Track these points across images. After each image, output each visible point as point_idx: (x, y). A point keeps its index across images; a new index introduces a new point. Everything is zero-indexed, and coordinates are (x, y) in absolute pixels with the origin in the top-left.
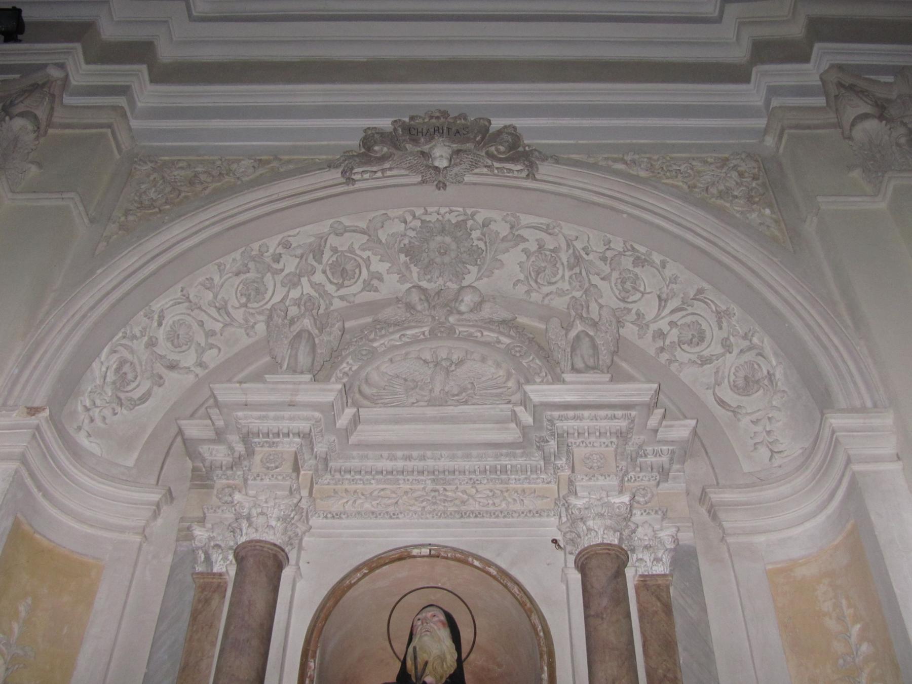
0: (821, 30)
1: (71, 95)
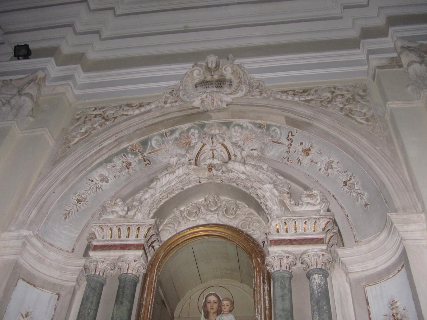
0: (394, 21)
1: (50, 81)
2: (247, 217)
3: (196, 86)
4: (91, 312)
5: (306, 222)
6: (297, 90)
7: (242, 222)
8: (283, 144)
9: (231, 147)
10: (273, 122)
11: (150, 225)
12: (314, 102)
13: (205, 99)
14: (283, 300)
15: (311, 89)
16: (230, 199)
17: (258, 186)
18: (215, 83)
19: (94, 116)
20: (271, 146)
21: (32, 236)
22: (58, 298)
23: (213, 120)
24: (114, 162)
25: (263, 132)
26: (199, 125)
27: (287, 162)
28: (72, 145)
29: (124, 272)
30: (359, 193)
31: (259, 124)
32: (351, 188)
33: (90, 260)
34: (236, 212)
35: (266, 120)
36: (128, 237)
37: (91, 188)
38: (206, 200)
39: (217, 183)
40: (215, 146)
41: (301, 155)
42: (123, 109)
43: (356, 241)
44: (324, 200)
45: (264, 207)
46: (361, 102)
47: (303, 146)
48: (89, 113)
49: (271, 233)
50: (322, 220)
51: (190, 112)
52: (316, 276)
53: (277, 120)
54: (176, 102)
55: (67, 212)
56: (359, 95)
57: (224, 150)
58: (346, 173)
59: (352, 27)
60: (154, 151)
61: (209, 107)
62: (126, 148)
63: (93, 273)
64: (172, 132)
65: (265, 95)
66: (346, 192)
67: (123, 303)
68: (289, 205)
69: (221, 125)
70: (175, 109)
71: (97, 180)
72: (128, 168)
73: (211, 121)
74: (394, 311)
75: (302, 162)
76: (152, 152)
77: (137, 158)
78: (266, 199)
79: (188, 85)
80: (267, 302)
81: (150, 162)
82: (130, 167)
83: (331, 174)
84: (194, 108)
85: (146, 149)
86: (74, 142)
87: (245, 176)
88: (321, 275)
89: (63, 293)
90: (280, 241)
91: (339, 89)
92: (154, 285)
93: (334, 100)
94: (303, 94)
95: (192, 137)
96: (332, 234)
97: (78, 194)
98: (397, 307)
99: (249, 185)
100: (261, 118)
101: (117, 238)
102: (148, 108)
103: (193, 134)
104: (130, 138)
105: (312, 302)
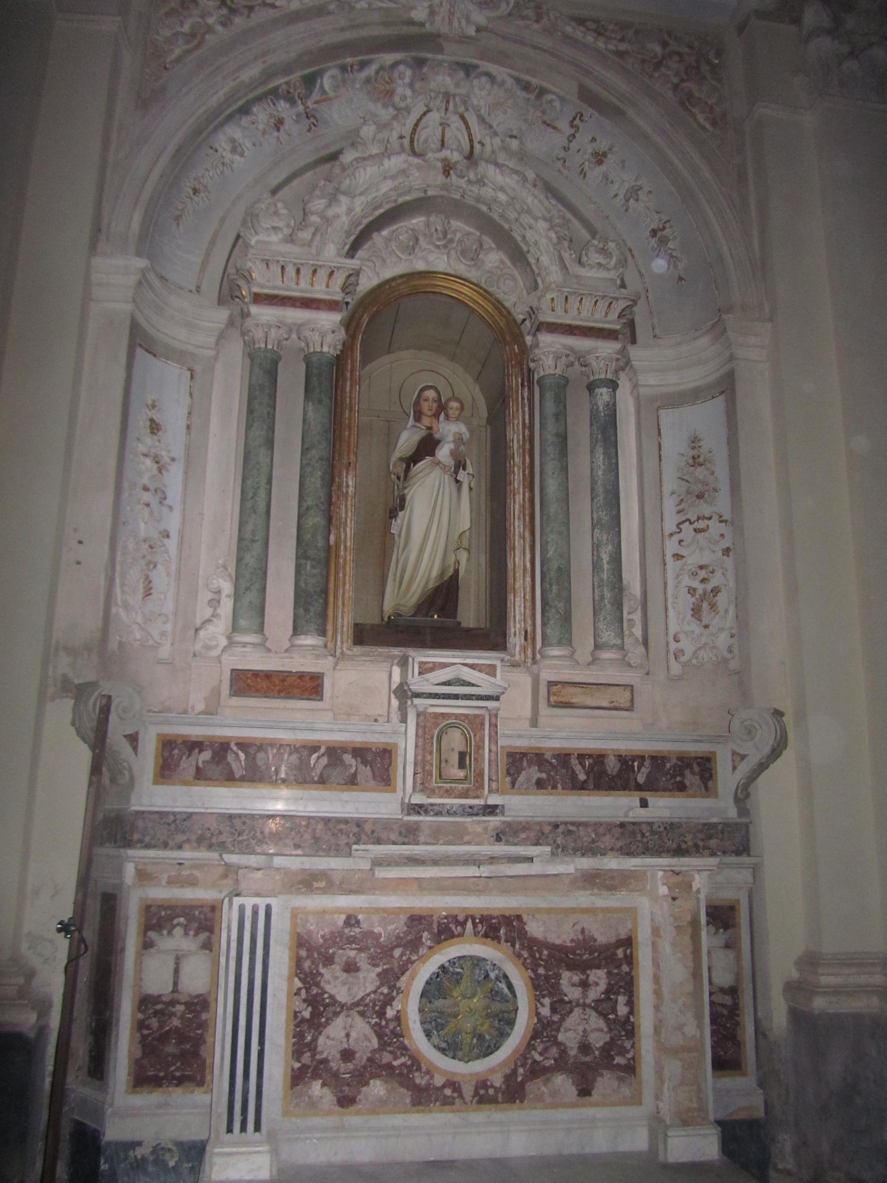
5: (597, 301)
6: (603, 23)
9: (476, 124)
11: (353, 269)
14: (557, 420)
16: (472, 230)
22: (192, 377)
26: (415, 59)
27: (562, 169)
28: (171, 62)
32: (663, 241)
36: (312, 285)
38: (428, 225)
40: (448, 119)
41: (588, 160)
43: (655, 336)
44: (622, 263)
45: (532, 261)
47: (593, 144)
51: (405, 30)
52: (604, 390)
55: (178, 213)
61: (445, 30)
62: (277, 88)
63: (263, 346)
64: (363, 65)
65: (545, 21)
66: (653, 248)
71: (224, 150)
72: (278, 130)
73: (439, 57)
74: (696, 452)
75: (588, 174)
77: (295, 110)
80: (527, 417)
84: (411, 22)
85: (311, 92)
86: (174, 56)
89: (198, 368)
95: (400, 82)
103: (401, 76)
104: (287, 69)
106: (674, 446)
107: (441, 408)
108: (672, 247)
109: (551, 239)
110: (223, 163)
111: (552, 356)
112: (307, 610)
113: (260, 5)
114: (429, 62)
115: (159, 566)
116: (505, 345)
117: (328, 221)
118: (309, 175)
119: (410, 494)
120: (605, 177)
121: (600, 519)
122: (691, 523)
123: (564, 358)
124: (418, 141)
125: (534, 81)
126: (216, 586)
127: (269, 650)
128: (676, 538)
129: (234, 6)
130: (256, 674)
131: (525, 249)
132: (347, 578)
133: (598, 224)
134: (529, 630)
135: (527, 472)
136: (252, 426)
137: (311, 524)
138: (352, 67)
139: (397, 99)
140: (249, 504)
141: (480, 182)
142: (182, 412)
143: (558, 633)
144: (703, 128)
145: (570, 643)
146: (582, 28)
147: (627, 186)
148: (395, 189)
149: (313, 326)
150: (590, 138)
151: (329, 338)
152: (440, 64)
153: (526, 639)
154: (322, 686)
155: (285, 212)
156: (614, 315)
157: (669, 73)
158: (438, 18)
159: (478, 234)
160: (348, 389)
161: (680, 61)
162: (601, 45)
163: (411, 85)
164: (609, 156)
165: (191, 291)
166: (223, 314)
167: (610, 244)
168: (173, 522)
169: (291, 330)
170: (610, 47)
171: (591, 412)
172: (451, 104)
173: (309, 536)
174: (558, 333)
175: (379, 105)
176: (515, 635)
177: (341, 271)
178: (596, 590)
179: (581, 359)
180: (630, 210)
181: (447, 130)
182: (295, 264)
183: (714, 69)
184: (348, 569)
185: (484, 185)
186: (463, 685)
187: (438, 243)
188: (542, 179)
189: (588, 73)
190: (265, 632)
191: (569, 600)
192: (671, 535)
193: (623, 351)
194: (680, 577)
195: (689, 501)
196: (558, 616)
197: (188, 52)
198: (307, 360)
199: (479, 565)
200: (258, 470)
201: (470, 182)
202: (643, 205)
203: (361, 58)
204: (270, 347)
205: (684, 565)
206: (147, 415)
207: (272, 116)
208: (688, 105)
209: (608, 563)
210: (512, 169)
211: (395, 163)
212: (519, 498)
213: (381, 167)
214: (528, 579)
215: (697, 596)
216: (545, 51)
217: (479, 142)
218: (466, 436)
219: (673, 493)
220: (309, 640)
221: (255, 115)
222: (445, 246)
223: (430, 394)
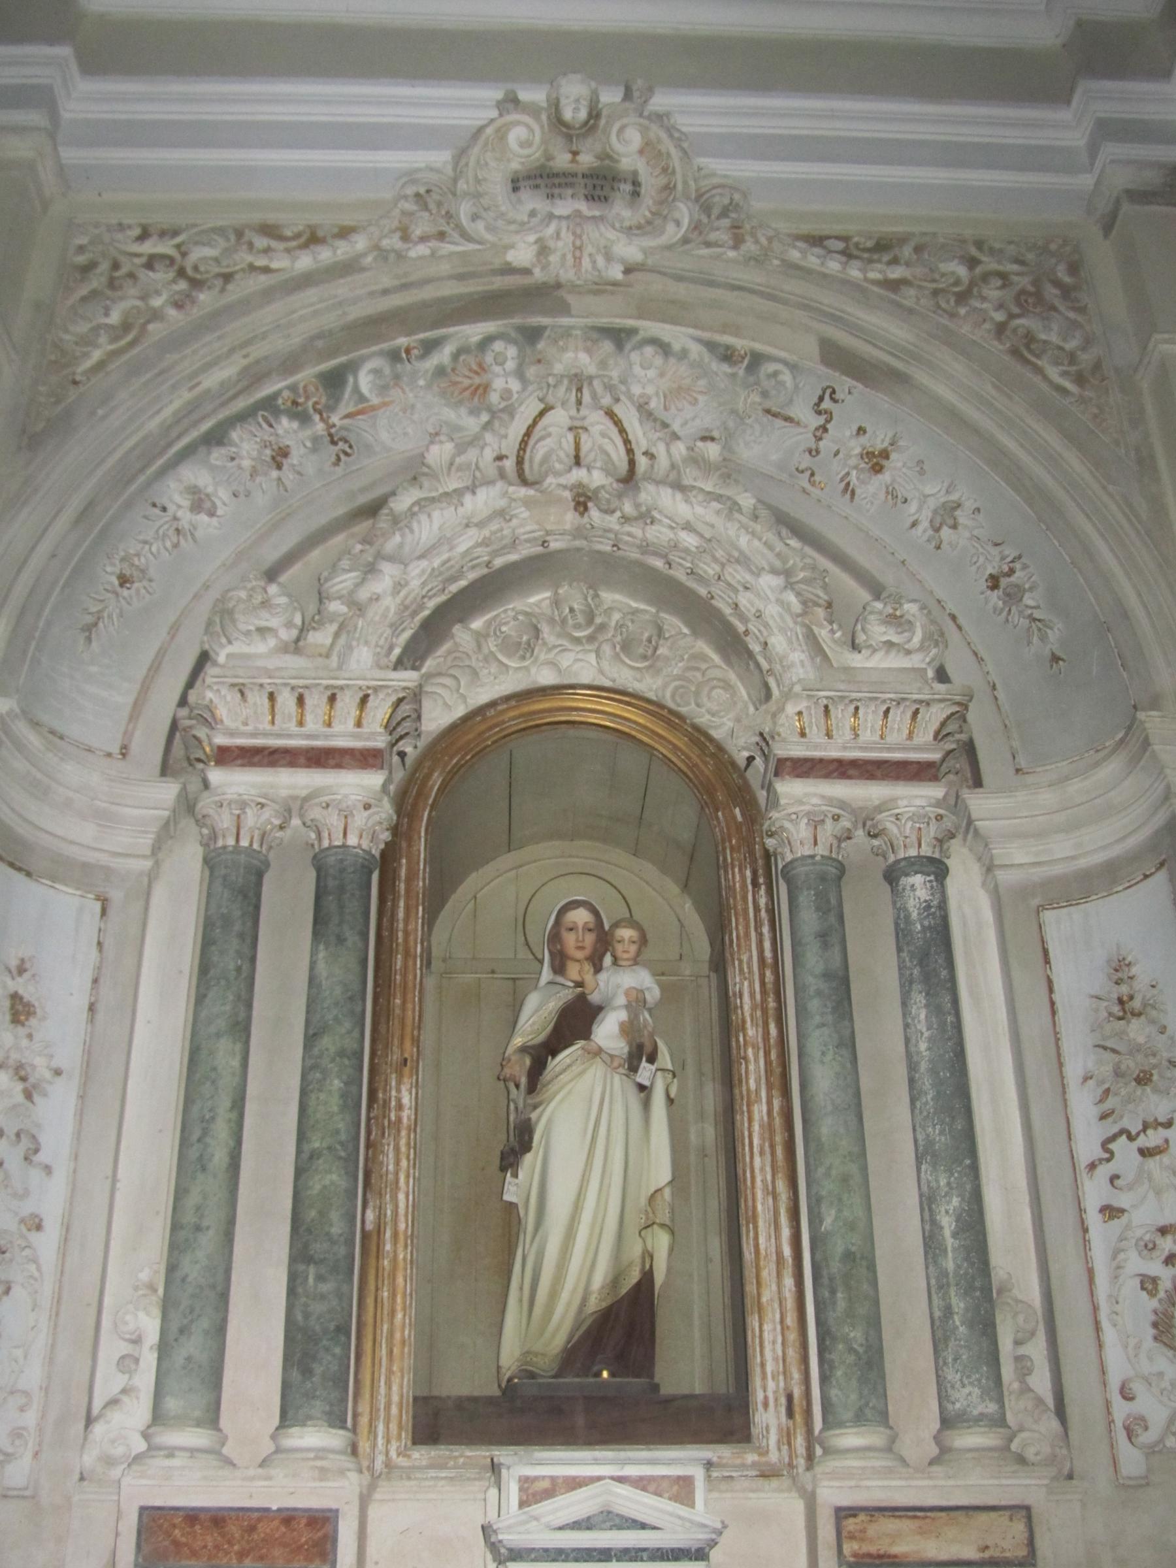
2: (688, 669)
3: (516, 184)
4: (244, 967)
5: (888, 710)
6: (856, 239)
7: (677, 683)
8: (798, 423)
9: (636, 424)
10: (776, 347)
11: (405, 688)
12: (912, 292)
13: (551, 244)
14: (825, 946)
15: (903, 240)
16: (642, 606)
17: (738, 577)
18: (582, 181)
19: (143, 260)
20: (757, 427)
21: (16, 716)
22: (104, 912)
23: (572, 316)
24: (232, 443)
25: (734, 375)
26: (521, 329)
28: (85, 373)
29: (337, 843)
30: (1035, 620)
31: (728, 347)
32: (1014, 596)
33: (217, 798)
34: (656, 649)
35: (753, 340)
36: (329, 725)
37: (161, 532)
38: (556, 603)
39: (599, 552)
40: (584, 418)
41: (856, 467)
42: (251, 245)
43: (1018, 771)
44: (936, 638)
45: (756, 648)
46: (1062, 308)
47: (863, 440)
48: (123, 247)
49: (783, 735)
50: (935, 708)
51: (499, 283)
52: (918, 879)
53: (793, 344)
54: (441, 236)
55: (89, 619)
56: (1057, 283)
57: (614, 432)
58: (999, 548)
59: (1042, 7)
60: (364, 409)
61: (567, 275)
63: (231, 842)
64: (429, 347)
65: (749, 246)
66: (995, 609)
67: (345, 940)
68: (830, 643)
69: (595, 335)
70: (445, 268)
71: (179, 507)
72: (279, 467)
73: (565, 321)
74: (1124, 989)
75: (858, 491)
76: (359, 413)
77: (309, 432)
78: (766, 625)
79: (485, 180)
80: (767, 945)
81: (351, 447)
82: (284, 461)
83: (950, 543)
84: (509, 270)
85: (338, 400)
86: (88, 364)
87: (697, 538)
88: (932, 878)
89: (116, 896)
90: (809, 764)
91: (992, 252)
92: (424, 879)
93: (975, 290)
94: (876, 257)
95: (497, 369)
96: (953, 746)
97: (122, 554)
98: (1131, 978)
99: (711, 572)
100: (737, 331)
101: (293, 727)
102: (342, 250)
103: (500, 360)
105: (904, 954)
106: (1078, 980)
107: (603, 944)
108: (1031, 603)
109: (789, 604)
110: (177, 530)
111: (805, 820)
112: (307, 1372)
113: (243, 270)
114: (547, 333)
115: (16, 1291)
116: (717, 810)
117: (359, 608)
118: (338, 540)
119: (542, 1120)
120: (891, 493)
121: (930, 1142)
122: (1131, 1138)
123: (829, 822)
124: (531, 461)
125: (740, 344)
126: (131, 1327)
127: (229, 1463)
128: (1104, 1171)
129: (198, 276)
130: (192, 1516)
131: (741, 628)
132: (399, 1300)
133: (888, 578)
134: (797, 1392)
135: (773, 1055)
136: (205, 996)
137: (318, 1187)
138: (408, 351)
139: (494, 398)
140: (193, 1153)
141: (646, 517)
142: (80, 981)
143: (853, 1396)
144: (1063, 391)
145: (883, 1418)
146: (817, 250)
147: (932, 503)
148: (485, 543)
149: (326, 798)
150: (855, 428)
151: (360, 819)
152: (567, 333)
153: (790, 1413)
154: (335, 1540)
155: (283, 600)
156: (925, 735)
157: (985, 306)
158: (553, 258)
159: (654, 610)
160: (401, 914)
161: (1004, 286)
162: (855, 273)
163: (520, 373)
164: (893, 456)
165: (109, 755)
166: (169, 791)
167: (906, 606)
168: (51, 1198)
169: (289, 811)
170: (872, 275)
171: (897, 924)
172: (586, 391)
173: (313, 1213)
174: (817, 777)
175: (463, 411)
176: (766, 1405)
177: (381, 695)
178: (934, 1297)
179: (868, 822)
180: (944, 546)
181: (584, 437)
182: (293, 688)
183: (1066, 291)
184: (400, 1280)
185: (652, 523)
186: (620, 1528)
187: (577, 634)
188: (769, 507)
189: (836, 319)
190: (223, 1423)
191: (875, 1322)
192: (1092, 1166)
193: (956, 805)
194: (1122, 1256)
195: (1123, 1092)
196: (851, 1359)
197: (114, 354)
198: (319, 863)
199: (708, 1260)
200: (213, 1082)
201: (626, 519)
202: (967, 534)
203: (422, 336)
204: (244, 843)
205: (1128, 1227)
206: (5, 987)
207: (266, 445)
208: (1026, 354)
209: (955, 1235)
210: (709, 493)
211: (483, 501)
212: (760, 1110)
213: (461, 510)
214: (789, 1282)
215: (1162, 1294)
216: (752, 291)
217: (645, 453)
218: (654, 994)
219: (1086, 1078)
220: (314, 1437)
221: (236, 445)
222: (591, 639)
223: (580, 916)
